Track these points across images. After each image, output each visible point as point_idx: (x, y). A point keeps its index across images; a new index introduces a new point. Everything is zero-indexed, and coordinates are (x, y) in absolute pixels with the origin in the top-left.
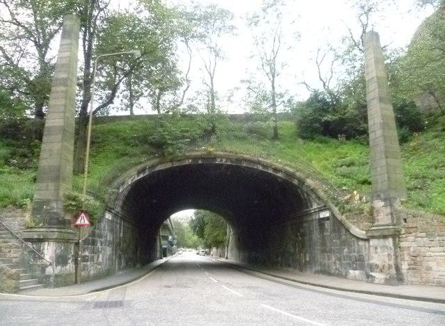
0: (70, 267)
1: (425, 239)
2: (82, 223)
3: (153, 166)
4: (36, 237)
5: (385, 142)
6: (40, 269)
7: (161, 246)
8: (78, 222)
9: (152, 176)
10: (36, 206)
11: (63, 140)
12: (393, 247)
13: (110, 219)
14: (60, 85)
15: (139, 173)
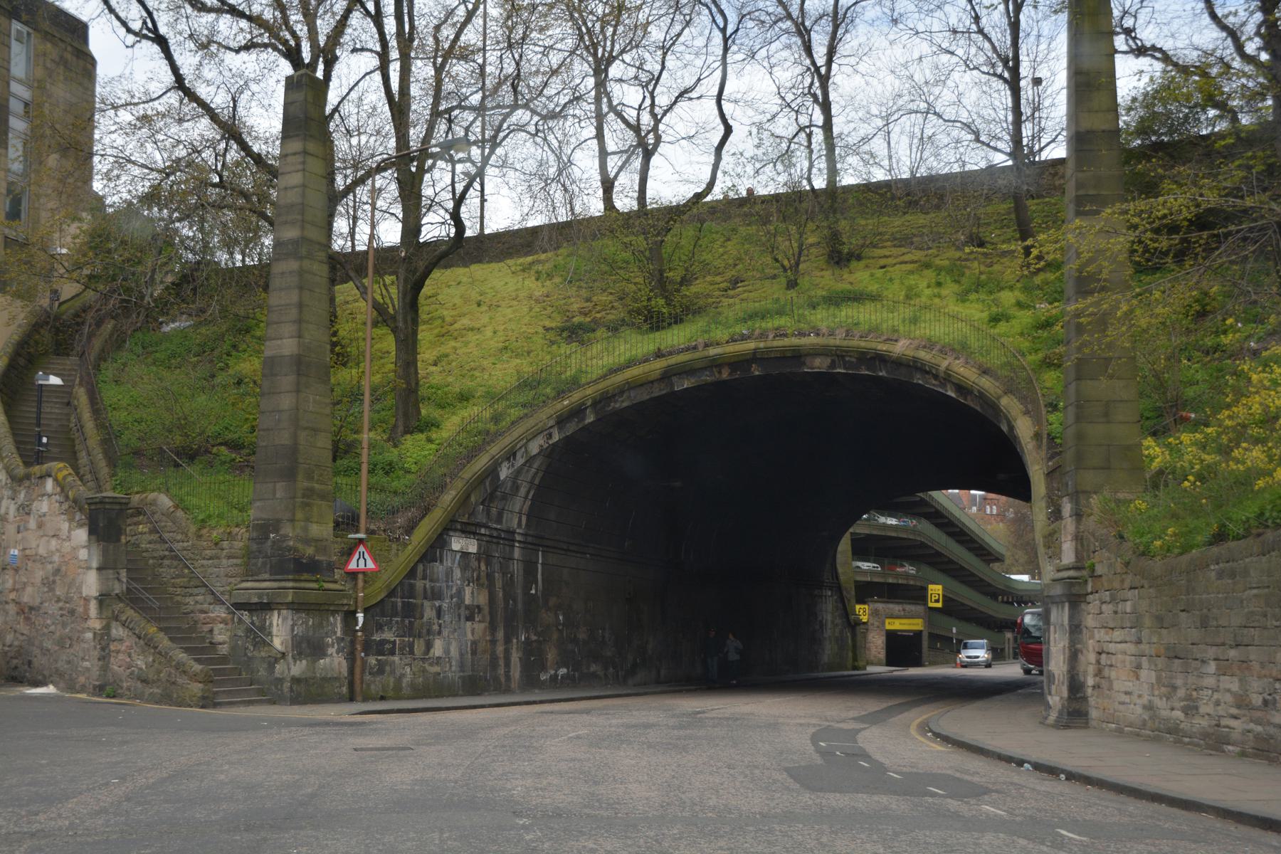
0: (334, 662)
2: (362, 566)
4: (255, 600)
8: (352, 566)
10: (255, 535)
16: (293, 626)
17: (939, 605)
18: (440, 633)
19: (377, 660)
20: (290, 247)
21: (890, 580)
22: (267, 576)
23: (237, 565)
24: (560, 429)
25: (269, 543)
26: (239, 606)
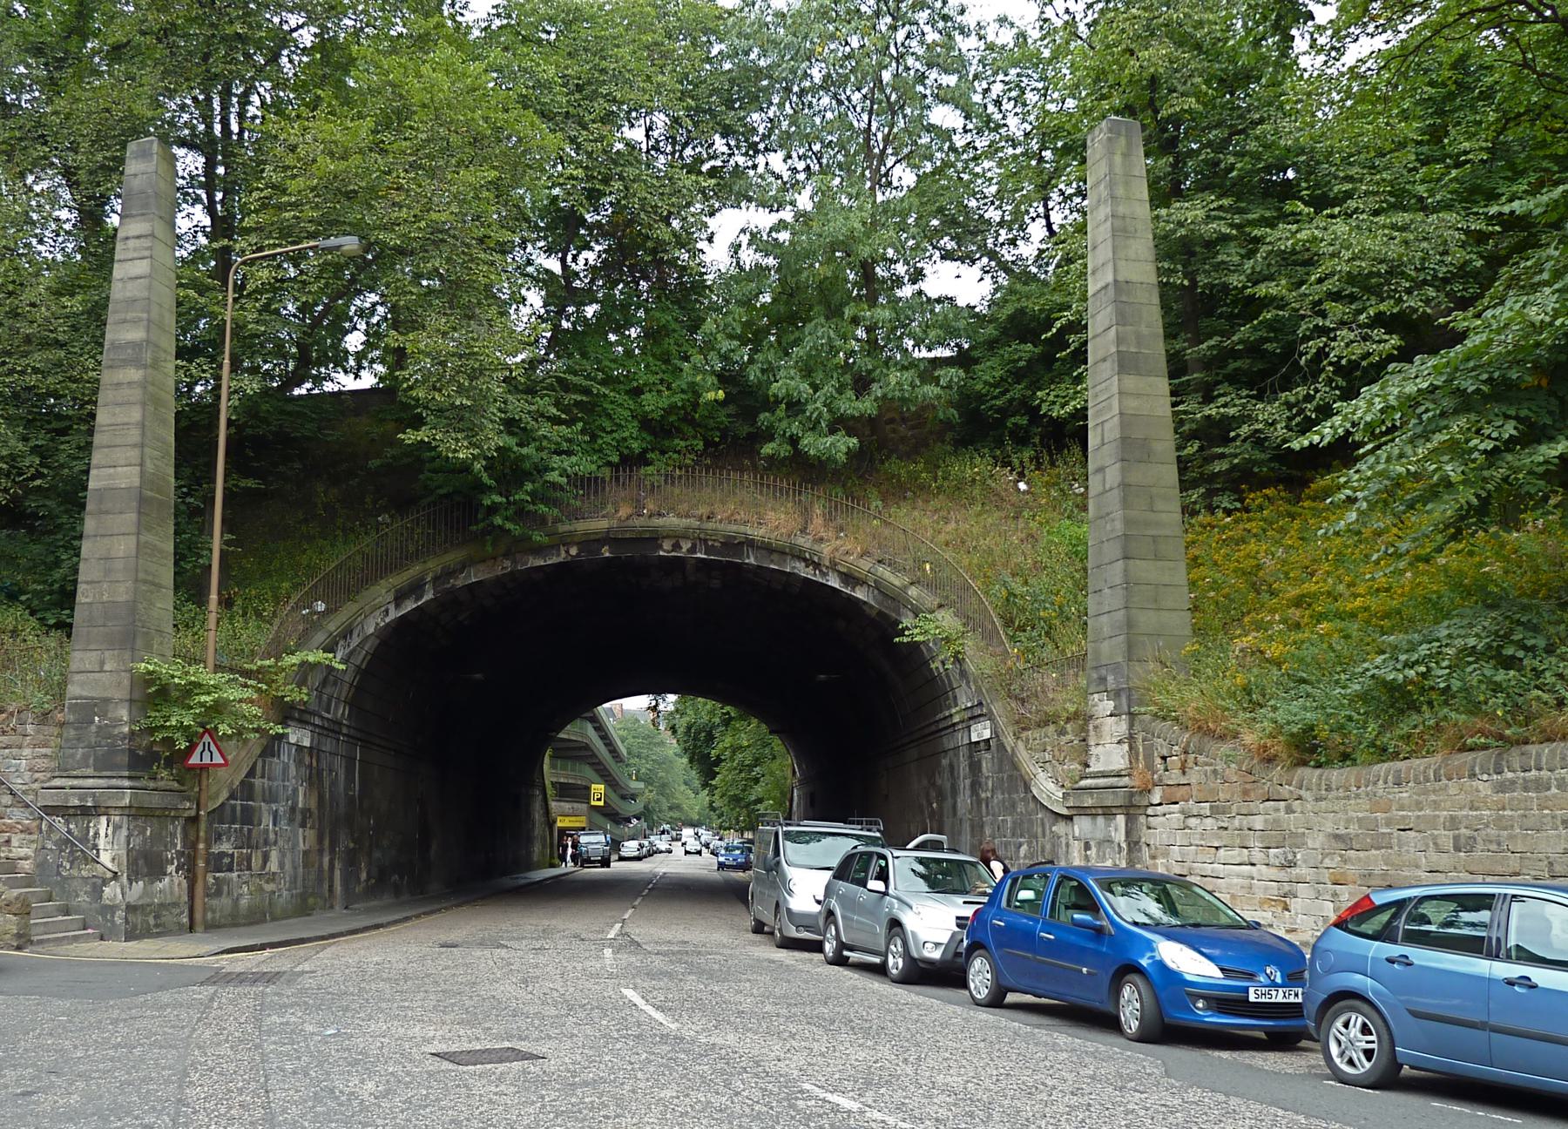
0: (172, 883)
1: (1209, 820)
2: (206, 760)
3: (449, 573)
5: (1125, 503)
6: (88, 888)
7: (551, 823)
9: (449, 601)
11: (141, 527)
12: (1124, 845)
13: (307, 743)
14: (126, 363)
15: (399, 599)
16: (128, 837)
17: (601, 803)
18: (275, 843)
19: (215, 878)
20: (129, 351)
21: (562, 780)
22: (90, 771)
23: (46, 756)
24: (397, 606)
25: (93, 728)
26: (51, 810)
